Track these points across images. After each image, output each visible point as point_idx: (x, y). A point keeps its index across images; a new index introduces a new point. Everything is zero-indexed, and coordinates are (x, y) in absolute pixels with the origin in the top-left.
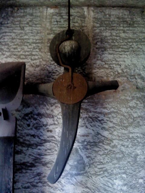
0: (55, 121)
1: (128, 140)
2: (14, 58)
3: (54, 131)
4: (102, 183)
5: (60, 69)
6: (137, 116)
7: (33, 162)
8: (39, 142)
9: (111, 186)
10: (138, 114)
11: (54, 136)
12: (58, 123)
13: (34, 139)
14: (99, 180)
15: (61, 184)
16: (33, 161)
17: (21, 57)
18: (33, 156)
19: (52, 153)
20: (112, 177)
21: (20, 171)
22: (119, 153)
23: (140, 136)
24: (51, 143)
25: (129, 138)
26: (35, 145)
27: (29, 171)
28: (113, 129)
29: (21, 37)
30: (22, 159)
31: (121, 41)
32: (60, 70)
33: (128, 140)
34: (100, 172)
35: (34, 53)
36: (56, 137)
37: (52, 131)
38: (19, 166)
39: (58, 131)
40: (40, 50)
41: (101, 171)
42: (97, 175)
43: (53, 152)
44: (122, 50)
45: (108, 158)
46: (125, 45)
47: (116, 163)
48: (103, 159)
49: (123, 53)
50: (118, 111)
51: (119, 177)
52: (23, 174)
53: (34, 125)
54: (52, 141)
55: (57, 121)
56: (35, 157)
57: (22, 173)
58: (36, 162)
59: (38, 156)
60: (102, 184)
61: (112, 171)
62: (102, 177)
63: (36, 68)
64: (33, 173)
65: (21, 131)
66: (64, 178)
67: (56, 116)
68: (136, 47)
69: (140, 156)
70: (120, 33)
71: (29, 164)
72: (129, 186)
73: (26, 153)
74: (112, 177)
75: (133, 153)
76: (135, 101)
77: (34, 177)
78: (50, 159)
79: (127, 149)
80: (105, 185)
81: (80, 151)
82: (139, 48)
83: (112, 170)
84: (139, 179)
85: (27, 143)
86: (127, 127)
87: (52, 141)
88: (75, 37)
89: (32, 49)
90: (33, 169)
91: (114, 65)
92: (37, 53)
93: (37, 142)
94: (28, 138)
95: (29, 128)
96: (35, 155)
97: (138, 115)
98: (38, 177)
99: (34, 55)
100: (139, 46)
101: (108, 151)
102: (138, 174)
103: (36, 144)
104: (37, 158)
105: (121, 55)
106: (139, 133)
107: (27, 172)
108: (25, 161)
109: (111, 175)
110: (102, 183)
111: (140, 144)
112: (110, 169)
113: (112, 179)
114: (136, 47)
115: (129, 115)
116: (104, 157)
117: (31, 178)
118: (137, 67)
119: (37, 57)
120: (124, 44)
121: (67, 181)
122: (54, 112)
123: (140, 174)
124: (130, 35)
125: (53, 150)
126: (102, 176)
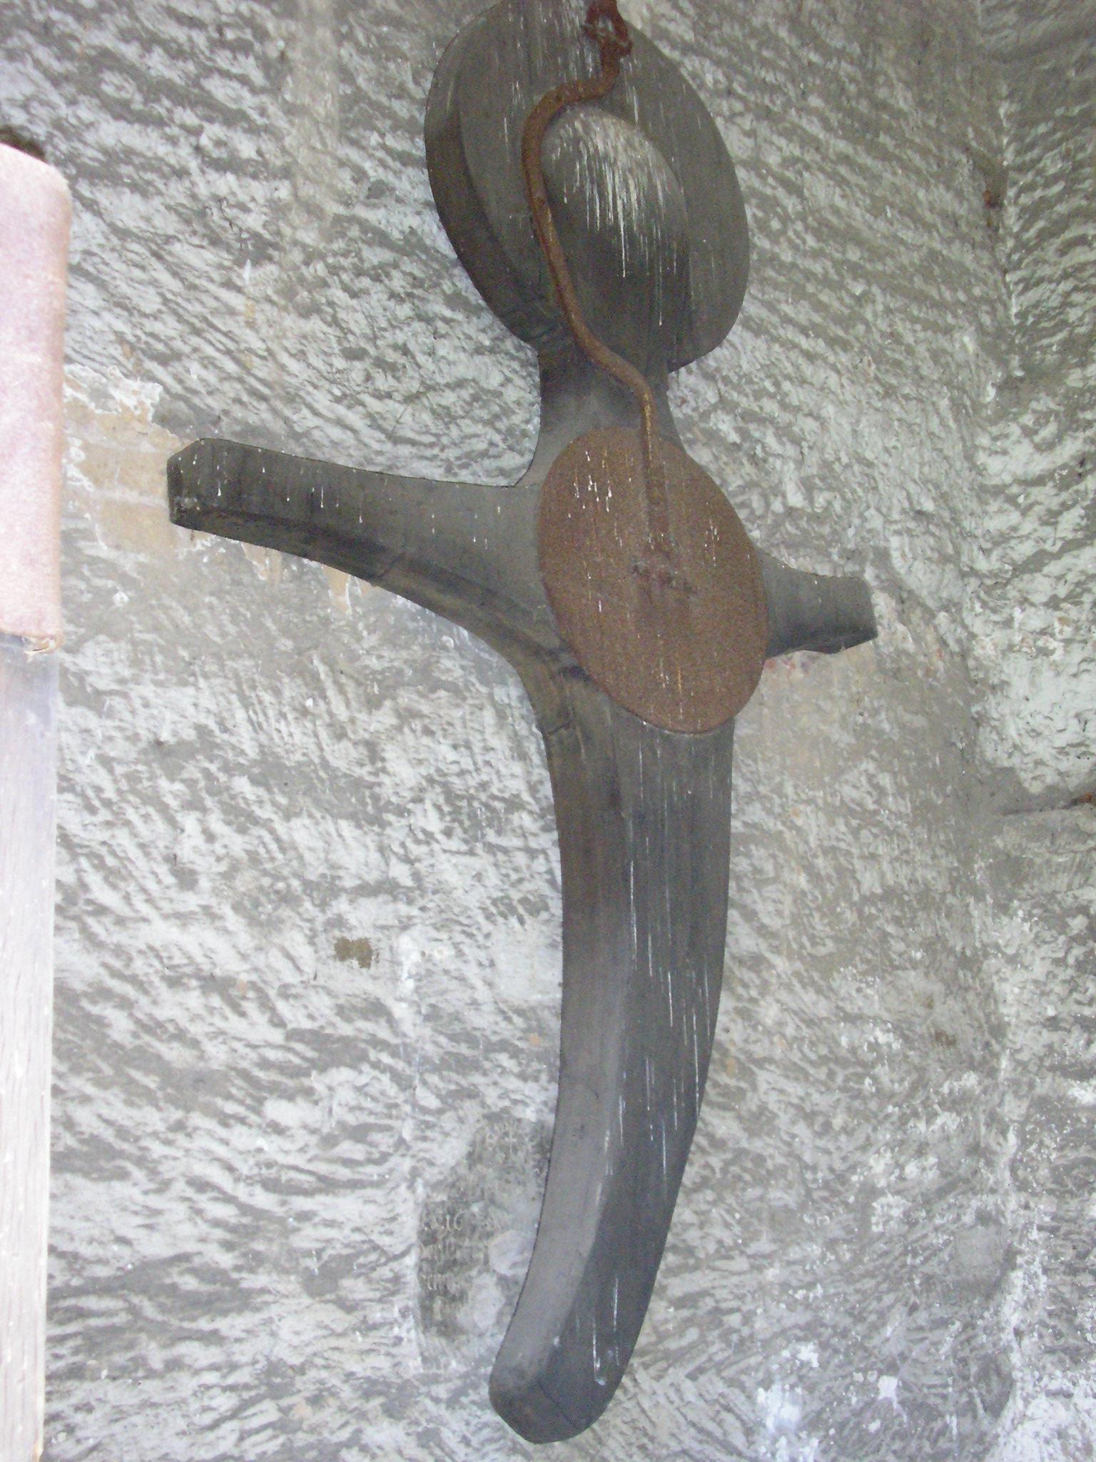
0: (393, 860)
1: (831, 1075)
2: (37, 63)
3: (385, 955)
4: (693, 1425)
5: (430, 341)
6: (879, 891)
7: (226, 1260)
8: (272, 1055)
9: (738, 1440)
10: (882, 875)
11: (389, 1002)
12: (416, 876)
13: (235, 1024)
14: (677, 1402)
15: (438, 1452)
16: (228, 1246)
17: (112, 83)
18: (229, 1199)
19: (372, 1171)
20: (745, 1371)
21: (120, 1358)
22: (781, 1171)
23: (889, 1045)
24: (365, 1067)
25: (837, 1060)
26: (237, 1087)
27: (193, 1351)
28: (753, 976)
29: (995, 439)
30: (128, 1226)
31: (811, 241)
32: (431, 353)
33: (831, 1075)
34: (681, 1331)
35: (219, 89)
36: (401, 1011)
37: (370, 952)
38: (107, 1303)
39: (416, 957)
40: (277, 69)
41: (688, 1322)
42: (667, 1355)
43: (384, 1157)
44: (817, 319)
45: (728, 1218)
46: (825, 282)
47: (764, 1256)
48: (701, 1226)
49: (820, 346)
50: (788, 835)
51: (782, 1367)
52: (152, 1388)
53: (228, 876)
54: (373, 1055)
55: (408, 860)
56: (245, 1209)
57: (135, 1370)
58: (255, 1262)
59: (263, 1200)
60: (692, 1431)
61: (748, 1319)
62: (692, 1376)
63: (240, 263)
64: (233, 1367)
65: (121, 921)
66: (464, 1400)
67: (401, 811)
68: (882, 325)
69: (883, 1200)
70: (807, 168)
71: (189, 1283)
72: (832, 1432)
73: (166, 1170)
74: (745, 1371)
75: (855, 1178)
76: (870, 766)
77: (235, 1414)
78: (359, 1223)
79: (821, 1143)
80: (709, 1434)
81: (415, 292)
82: (895, 337)
83: (745, 1308)
84: (881, 1373)
85: (174, 1054)
86: (827, 966)
87: (373, 1055)
88: (639, 92)
89: (200, 39)
90: (230, 1325)
91: (771, 440)
92: (249, 102)
93: (253, 1055)
94: (174, 1006)
95: (191, 901)
96: (241, 1192)
97: (882, 885)
98: (268, 1411)
99: (232, 118)
100: (900, 328)
101: (729, 1156)
102: (876, 1341)
103: (245, 1075)
104: (258, 1214)
105: (810, 357)
106: (885, 1022)
107: (174, 1365)
108: (155, 1247)
109: (743, 1347)
110: (695, 1419)
111: (890, 1109)
112: (734, 1304)
113: (748, 1381)
114: (882, 325)
115: (840, 871)
116: (704, 1207)
117: (208, 1419)
118: (875, 489)
119: (246, 148)
120: (826, 273)
121: (486, 1425)
122: (389, 766)
123: (888, 1340)
124: (857, 212)
125: (384, 1141)
126: (690, 1368)
